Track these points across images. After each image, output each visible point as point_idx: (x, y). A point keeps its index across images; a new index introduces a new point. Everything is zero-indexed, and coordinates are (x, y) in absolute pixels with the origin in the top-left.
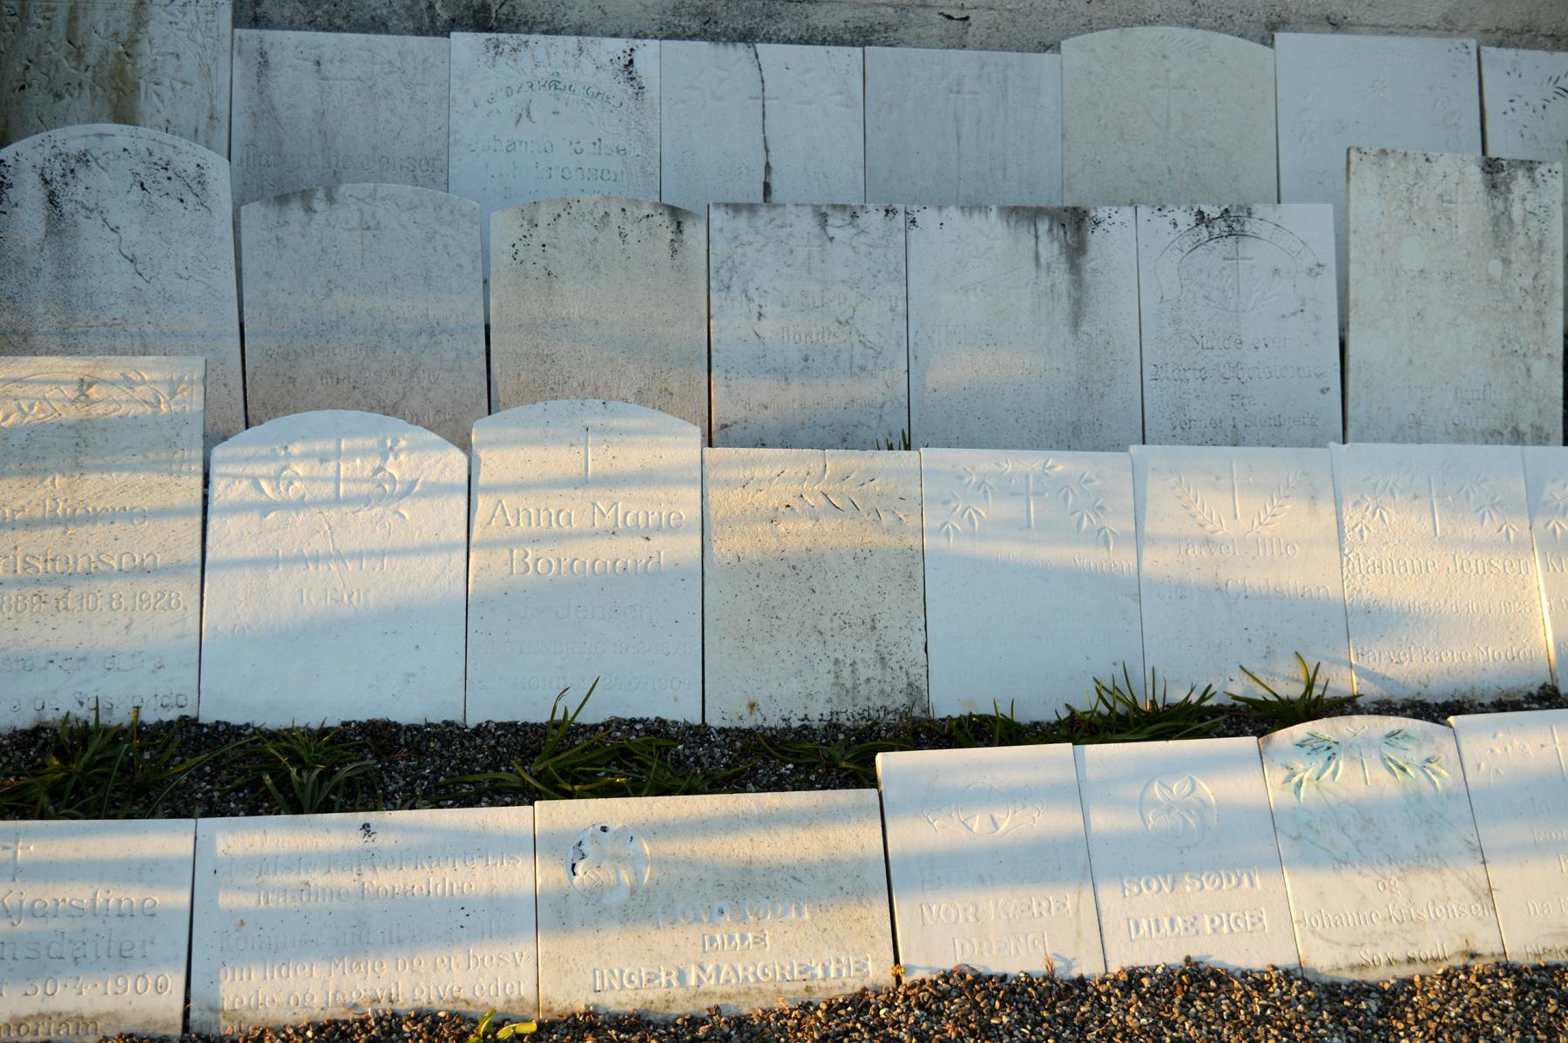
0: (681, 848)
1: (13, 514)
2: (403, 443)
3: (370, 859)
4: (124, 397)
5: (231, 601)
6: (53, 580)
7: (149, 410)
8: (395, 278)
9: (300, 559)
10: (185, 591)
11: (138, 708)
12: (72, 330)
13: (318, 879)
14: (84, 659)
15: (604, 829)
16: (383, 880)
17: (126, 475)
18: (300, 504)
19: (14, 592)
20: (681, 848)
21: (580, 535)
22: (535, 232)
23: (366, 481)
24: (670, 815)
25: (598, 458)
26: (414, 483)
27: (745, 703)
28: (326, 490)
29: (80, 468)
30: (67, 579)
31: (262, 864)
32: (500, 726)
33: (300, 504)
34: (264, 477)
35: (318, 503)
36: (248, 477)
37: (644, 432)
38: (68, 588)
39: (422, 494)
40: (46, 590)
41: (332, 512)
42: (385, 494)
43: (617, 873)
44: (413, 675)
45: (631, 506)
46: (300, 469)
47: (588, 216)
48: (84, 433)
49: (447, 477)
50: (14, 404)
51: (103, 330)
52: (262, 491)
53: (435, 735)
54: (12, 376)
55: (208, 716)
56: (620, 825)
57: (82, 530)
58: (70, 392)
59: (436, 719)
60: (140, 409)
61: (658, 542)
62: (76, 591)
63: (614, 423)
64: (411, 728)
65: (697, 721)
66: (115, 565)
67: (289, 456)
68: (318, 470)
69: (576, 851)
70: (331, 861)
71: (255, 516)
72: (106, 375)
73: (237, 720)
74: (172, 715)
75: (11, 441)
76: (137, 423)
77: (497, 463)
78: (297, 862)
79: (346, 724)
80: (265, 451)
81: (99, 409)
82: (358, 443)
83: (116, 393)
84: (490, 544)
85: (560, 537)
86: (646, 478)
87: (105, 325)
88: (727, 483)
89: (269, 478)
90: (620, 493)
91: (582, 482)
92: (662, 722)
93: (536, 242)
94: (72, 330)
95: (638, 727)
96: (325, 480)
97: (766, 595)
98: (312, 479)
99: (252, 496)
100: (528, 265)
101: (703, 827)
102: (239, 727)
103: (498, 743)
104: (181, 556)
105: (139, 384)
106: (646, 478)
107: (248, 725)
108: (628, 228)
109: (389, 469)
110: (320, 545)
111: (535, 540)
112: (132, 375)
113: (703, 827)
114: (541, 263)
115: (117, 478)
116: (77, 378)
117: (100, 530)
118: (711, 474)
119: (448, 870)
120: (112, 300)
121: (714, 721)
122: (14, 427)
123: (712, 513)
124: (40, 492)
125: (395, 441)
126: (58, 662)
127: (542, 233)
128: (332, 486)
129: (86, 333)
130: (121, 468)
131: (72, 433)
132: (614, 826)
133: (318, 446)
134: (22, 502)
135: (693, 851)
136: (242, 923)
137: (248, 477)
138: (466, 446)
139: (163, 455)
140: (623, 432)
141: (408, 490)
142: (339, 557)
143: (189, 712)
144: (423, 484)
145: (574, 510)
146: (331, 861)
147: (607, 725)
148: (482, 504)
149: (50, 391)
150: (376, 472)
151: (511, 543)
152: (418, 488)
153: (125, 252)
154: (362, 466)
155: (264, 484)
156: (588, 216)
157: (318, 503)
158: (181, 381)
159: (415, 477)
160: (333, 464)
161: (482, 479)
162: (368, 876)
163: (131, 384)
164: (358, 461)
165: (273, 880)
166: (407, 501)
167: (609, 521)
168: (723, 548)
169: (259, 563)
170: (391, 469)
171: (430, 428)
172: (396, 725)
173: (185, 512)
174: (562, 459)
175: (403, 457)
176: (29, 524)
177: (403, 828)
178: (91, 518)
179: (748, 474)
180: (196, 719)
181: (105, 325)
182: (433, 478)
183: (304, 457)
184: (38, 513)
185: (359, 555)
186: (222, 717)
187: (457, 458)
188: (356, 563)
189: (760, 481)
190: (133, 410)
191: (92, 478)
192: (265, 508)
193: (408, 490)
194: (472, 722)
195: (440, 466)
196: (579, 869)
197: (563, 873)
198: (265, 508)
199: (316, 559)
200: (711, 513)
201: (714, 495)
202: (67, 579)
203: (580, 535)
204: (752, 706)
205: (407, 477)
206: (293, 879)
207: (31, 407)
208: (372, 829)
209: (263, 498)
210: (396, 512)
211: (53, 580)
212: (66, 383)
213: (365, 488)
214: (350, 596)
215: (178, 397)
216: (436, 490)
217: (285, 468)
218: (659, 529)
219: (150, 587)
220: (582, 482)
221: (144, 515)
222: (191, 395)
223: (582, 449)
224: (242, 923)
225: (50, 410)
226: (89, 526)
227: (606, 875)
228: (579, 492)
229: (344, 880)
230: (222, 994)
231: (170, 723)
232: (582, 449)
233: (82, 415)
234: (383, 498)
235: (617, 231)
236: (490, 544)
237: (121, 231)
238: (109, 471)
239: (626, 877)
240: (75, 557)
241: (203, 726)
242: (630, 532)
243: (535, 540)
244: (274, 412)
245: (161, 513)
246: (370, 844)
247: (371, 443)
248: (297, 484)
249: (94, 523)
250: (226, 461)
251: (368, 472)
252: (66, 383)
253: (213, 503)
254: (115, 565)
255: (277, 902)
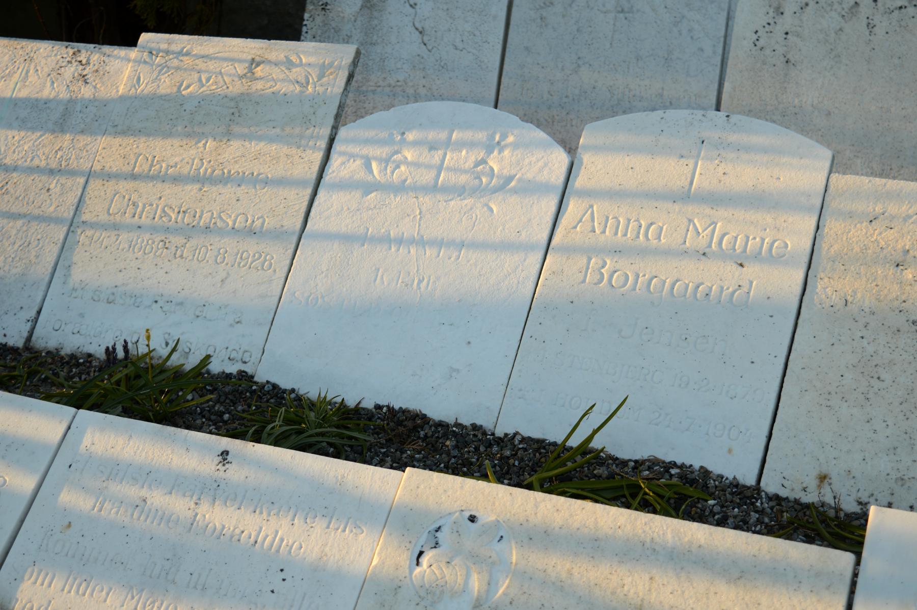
0: (557, 565)
1: (167, 169)
2: (511, 139)
3: (213, 490)
4: (281, 76)
5: (318, 272)
6: (178, 231)
7: (298, 88)
8: (638, 58)
9: (386, 240)
10: (279, 255)
11: (148, 330)
12: (364, 88)
13: (157, 498)
14: (181, 304)
15: (472, 519)
16: (219, 516)
17: (262, 144)
18: (399, 188)
19: (147, 236)
20: (557, 565)
21: (667, 253)
22: (780, 20)
23: (465, 172)
24: (558, 520)
25: (706, 174)
26: (510, 179)
27: (814, 473)
28: (427, 177)
29: (229, 135)
30: (189, 231)
31: (114, 469)
32: (524, 440)
33: (399, 188)
34: (375, 159)
35: (419, 189)
36: (362, 157)
37: (765, 150)
38: (188, 238)
39: (515, 191)
40: (171, 238)
41: (427, 199)
42: (484, 187)
43: (468, 576)
44: (458, 371)
45: (732, 228)
46: (409, 155)
47: (836, 6)
48: (241, 105)
49: (544, 177)
50: (196, 76)
51: (387, 89)
52: (371, 172)
53: (455, 434)
54: (202, 53)
55: (261, 377)
56: (492, 518)
57: (214, 189)
58: (241, 69)
59: (466, 421)
60: (291, 88)
61: (751, 270)
62: (193, 242)
63: (733, 138)
64: (441, 424)
65: (751, 481)
66: (231, 223)
67: (403, 141)
68: (426, 157)
69: (430, 535)
70: (177, 483)
71: (357, 194)
72: (273, 56)
73: (285, 383)
74: (232, 369)
75: (185, 107)
76: (285, 100)
77: (597, 168)
78: (147, 475)
79: (378, 407)
80: (384, 135)
81: (259, 85)
82: (468, 135)
83: (276, 72)
84: (569, 250)
85: (644, 252)
86: (756, 200)
87: (389, 86)
88: (851, 215)
89: (380, 160)
90: (722, 213)
91: (685, 196)
92: (705, 473)
93: (779, 30)
94: (364, 88)
95: (673, 471)
96: (429, 167)
97: (870, 349)
98: (416, 165)
99: (361, 175)
100: (768, 52)
101: (594, 546)
102: (284, 391)
103: (514, 456)
104: (285, 223)
105: (297, 66)
106: (756, 200)
107: (293, 391)
108: (877, 19)
109: (491, 163)
110: (407, 229)
111: (617, 251)
112: (294, 58)
113: (594, 546)
114: (781, 50)
115: (255, 147)
116: (250, 57)
117: (228, 192)
118: (832, 204)
119: (285, 522)
120: (399, 66)
121: (770, 485)
122: (191, 96)
123: (825, 246)
124: (193, 152)
125: (504, 136)
126: (160, 303)
127: (787, 23)
128: (433, 173)
129: (374, 92)
130: (260, 138)
131: (232, 104)
132: (486, 517)
133: (431, 135)
134: (177, 159)
135: (570, 573)
136: (69, 525)
137: (362, 157)
138: (571, 149)
139: (297, 130)
140: (748, 149)
141: (504, 186)
142: (421, 243)
143: (249, 369)
144: (519, 180)
145: (668, 225)
146: (177, 483)
147: (638, 463)
148: (573, 207)
149: (227, 68)
150: (477, 164)
151: (590, 251)
152: (513, 184)
153: (417, 25)
154: (467, 158)
155: (374, 165)
156: (836, 6)
157: (419, 189)
158: (331, 65)
159: (513, 172)
160: (440, 152)
161: (579, 182)
162: (204, 508)
163: (289, 64)
164: (464, 152)
165: (115, 488)
166: (499, 196)
167: (702, 242)
168: (826, 288)
169: (347, 239)
170: (494, 163)
171: (539, 125)
172: (424, 417)
173: (299, 183)
174: (668, 171)
175: (506, 153)
176: (177, 179)
177: (259, 464)
178: (224, 180)
179: (879, 208)
180: (252, 377)
181: (389, 86)
182: (529, 176)
183: (416, 143)
184: (185, 170)
185: (439, 244)
186: (274, 379)
187: (560, 158)
188: (434, 251)
189: (892, 218)
190: (284, 88)
191: (236, 144)
192: (369, 188)
193: (504, 186)
194: (499, 433)
195: (540, 164)
196: (425, 560)
197: (404, 558)
198: (369, 188)
199: (400, 241)
200: (824, 247)
201: (832, 226)
202: (189, 231)
203: (667, 253)
204: (823, 478)
205: (506, 172)
206: (133, 492)
207: (208, 80)
208: (229, 458)
209: (370, 178)
210: (487, 205)
211: (178, 231)
212: (240, 61)
213: (463, 179)
214: (420, 282)
215: (325, 79)
216: (530, 188)
217: (397, 152)
218: (757, 257)
219: (251, 247)
220: (685, 196)
221: (267, 182)
222: (335, 79)
223: (691, 162)
224: (69, 525)
225: (222, 83)
226: (220, 186)
227: (453, 575)
228: (677, 207)
229: (180, 505)
230: (19, 595)
231: (229, 376)
232: (691, 162)
233: (243, 90)
234: (477, 191)
235: (865, 21)
236: (569, 250)
237: (417, 7)
238: (250, 140)
239: (476, 584)
240: (202, 212)
241: (256, 383)
242: (723, 256)
243: (617, 251)
244: (401, 94)
245: (281, 182)
246: (221, 473)
247: (481, 136)
248: (403, 168)
249: (226, 184)
250: (347, 141)
251: (470, 164)
252: (240, 61)
253: (327, 178)
254: (231, 223)
255: (110, 512)
